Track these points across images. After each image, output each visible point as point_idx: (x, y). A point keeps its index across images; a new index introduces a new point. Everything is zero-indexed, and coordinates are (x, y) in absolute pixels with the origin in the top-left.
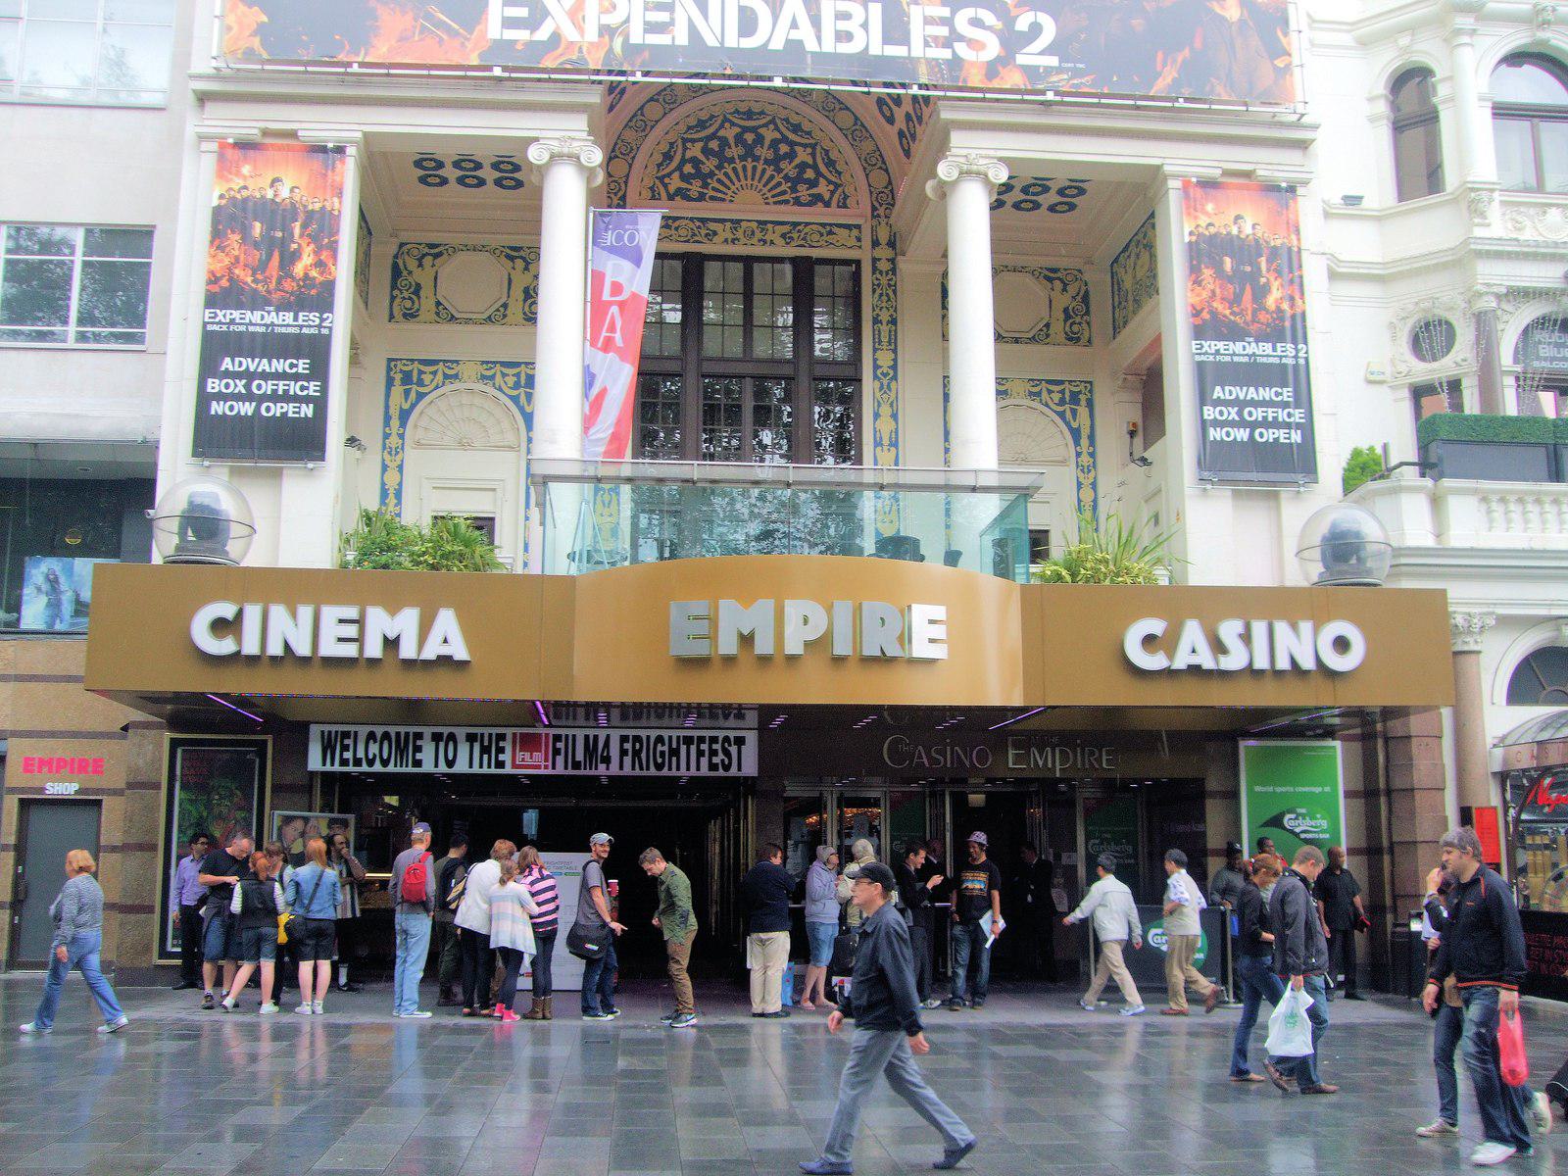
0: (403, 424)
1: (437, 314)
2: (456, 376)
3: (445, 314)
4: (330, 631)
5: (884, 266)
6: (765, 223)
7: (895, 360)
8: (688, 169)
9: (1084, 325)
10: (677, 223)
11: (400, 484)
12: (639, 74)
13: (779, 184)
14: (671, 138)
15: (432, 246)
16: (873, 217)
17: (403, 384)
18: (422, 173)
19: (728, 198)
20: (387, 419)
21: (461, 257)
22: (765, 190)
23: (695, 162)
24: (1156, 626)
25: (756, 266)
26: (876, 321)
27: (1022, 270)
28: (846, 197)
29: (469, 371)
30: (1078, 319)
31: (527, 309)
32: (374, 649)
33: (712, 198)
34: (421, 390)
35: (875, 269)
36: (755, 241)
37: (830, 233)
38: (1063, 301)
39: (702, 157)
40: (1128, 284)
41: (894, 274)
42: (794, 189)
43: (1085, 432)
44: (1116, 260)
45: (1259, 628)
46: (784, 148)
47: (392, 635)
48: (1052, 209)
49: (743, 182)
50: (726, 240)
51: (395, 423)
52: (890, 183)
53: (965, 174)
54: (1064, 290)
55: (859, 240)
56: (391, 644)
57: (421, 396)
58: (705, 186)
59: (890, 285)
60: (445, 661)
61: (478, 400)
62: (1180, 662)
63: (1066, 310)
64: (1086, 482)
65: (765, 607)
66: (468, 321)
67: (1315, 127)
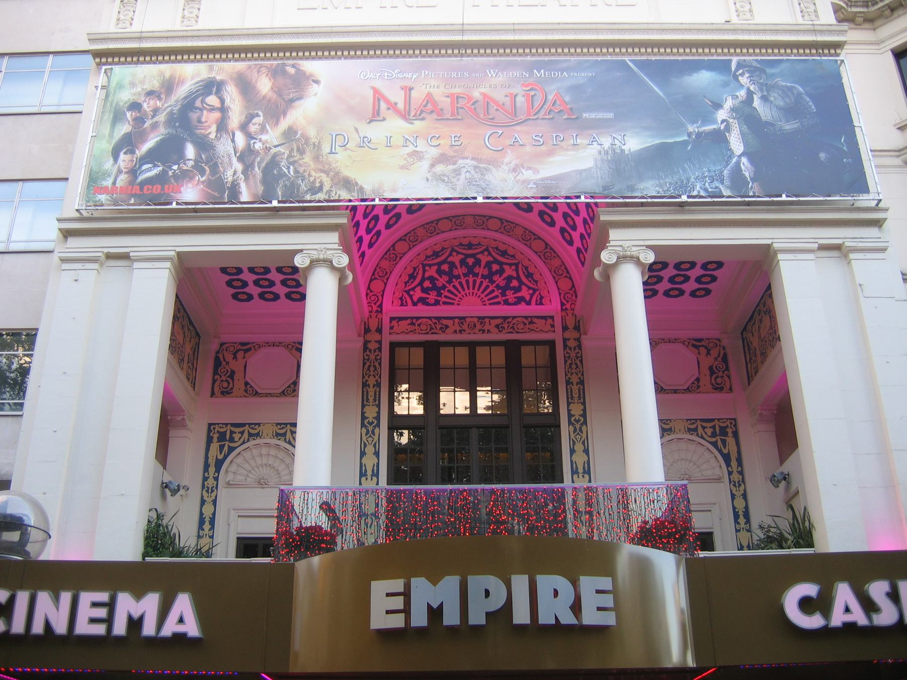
0: (218, 470)
1: (246, 391)
2: (258, 435)
3: (250, 391)
4: (85, 611)
5: (572, 343)
6: (484, 318)
7: (584, 410)
8: (427, 284)
9: (726, 378)
10: (419, 321)
11: (214, 514)
12: (377, 200)
13: (493, 291)
14: (414, 264)
15: (243, 344)
16: (562, 310)
17: (219, 441)
18: (233, 291)
19: (456, 302)
20: (206, 466)
21: (264, 351)
22: (482, 296)
23: (432, 279)
24: (810, 589)
26: (568, 383)
27: (676, 340)
28: (542, 298)
29: (268, 430)
30: (720, 374)
31: (713, 381)
32: (120, 628)
33: (444, 303)
34: (232, 445)
35: (565, 346)
36: (476, 330)
37: (531, 323)
38: (707, 362)
39: (436, 276)
40: (755, 342)
41: (581, 349)
42: (503, 295)
43: (734, 456)
44: (745, 329)
46: (495, 267)
47: (136, 615)
48: (693, 294)
49: (467, 291)
50: (455, 332)
51: (212, 469)
52: (573, 286)
53: (623, 259)
54: (708, 353)
55: (553, 326)
56: (135, 624)
57: (231, 449)
58: (439, 295)
59: (577, 357)
60: (180, 639)
61: (273, 452)
62: (838, 619)
63: (711, 368)
64: (738, 494)
65: (451, 583)
66: (267, 395)
67: (886, 210)
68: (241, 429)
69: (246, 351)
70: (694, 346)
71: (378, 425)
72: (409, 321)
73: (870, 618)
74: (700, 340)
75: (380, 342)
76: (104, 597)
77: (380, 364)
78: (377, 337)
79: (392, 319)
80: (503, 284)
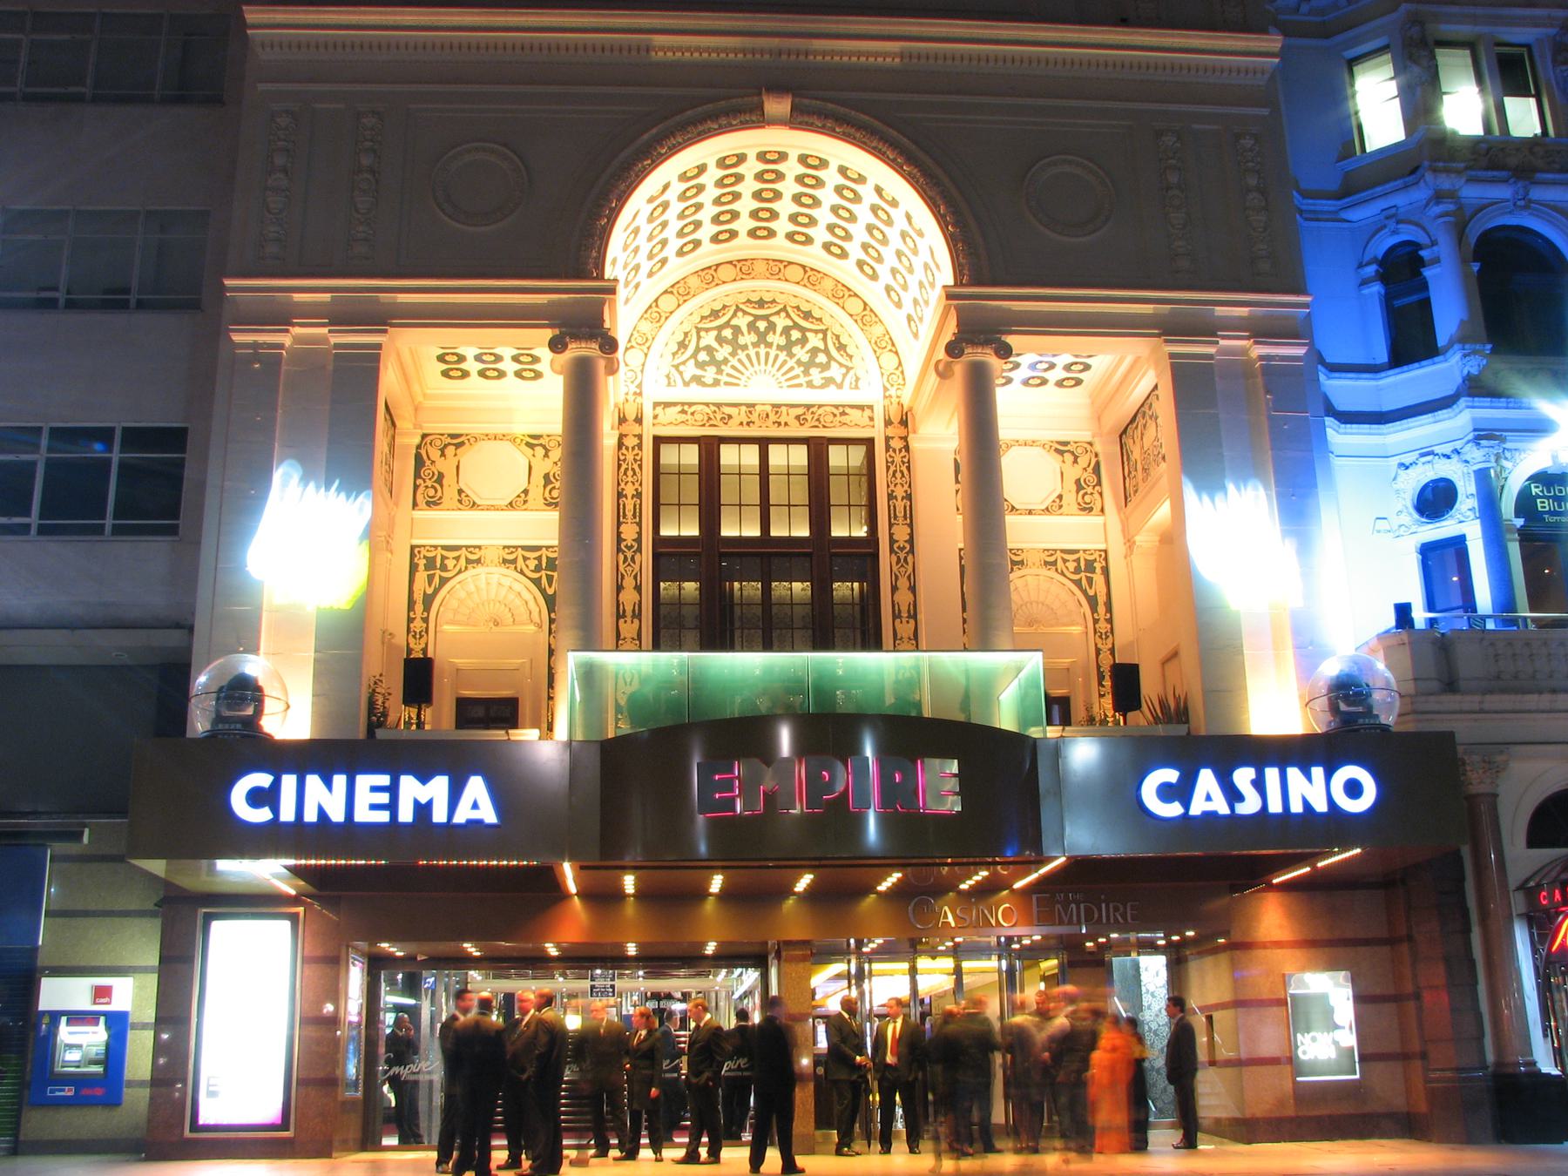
0: (427, 608)
1: (460, 502)
2: (478, 561)
3: (465, 501)
4: (364, 798)
9: (1097, 496)
10: (693, 408)
13: (792, 369)
14: (687, 327)
15: (453, 436)
25: (772, 448)
28: (857, 379)
30: (1089, 490)
32: (406, 815)
33: (726, 384)
34: (445, 575)
35: (888, 448)
37: (843, 414)
38: (1074, 472)
40: (1136, 454)
42: (806, 373)
43: (1102, 599)
45: (1272, 774)
47: (423, 801)
48: (1060, 384)
51: (419, 607)
54: (1075, 461)
55: (871, 419)
56: (422, 810)
57: (444, 581)
58: (720, 372)
62: (1198, 807)
68: (456, 554)
69: (458, 446)
70: (1057, 450)
71: (639, 550)
72: (679, 408)
73: (1232, 808)
74: (1065, 444)
75: (640, 437)
76: (384, 780)
77: (640, 467)
78: (636, 429)
79: (656, 405)
80: (805, 358)
